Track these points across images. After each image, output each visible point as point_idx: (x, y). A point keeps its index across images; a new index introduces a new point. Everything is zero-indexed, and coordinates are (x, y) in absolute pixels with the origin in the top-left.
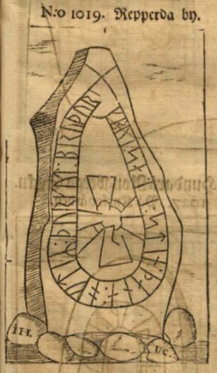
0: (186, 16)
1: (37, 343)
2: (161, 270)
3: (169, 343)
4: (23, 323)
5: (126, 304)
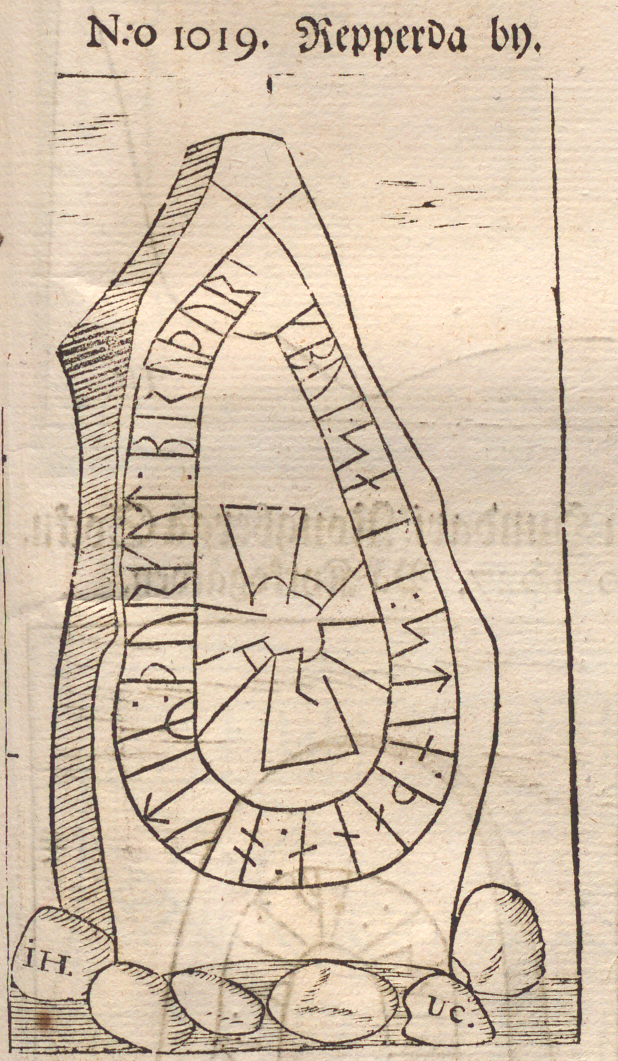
0: (501, 40)
1: (88, 993)
2: (438, 776)
3: (469, 987)
4: (52, 936)
5: (344, 877)
